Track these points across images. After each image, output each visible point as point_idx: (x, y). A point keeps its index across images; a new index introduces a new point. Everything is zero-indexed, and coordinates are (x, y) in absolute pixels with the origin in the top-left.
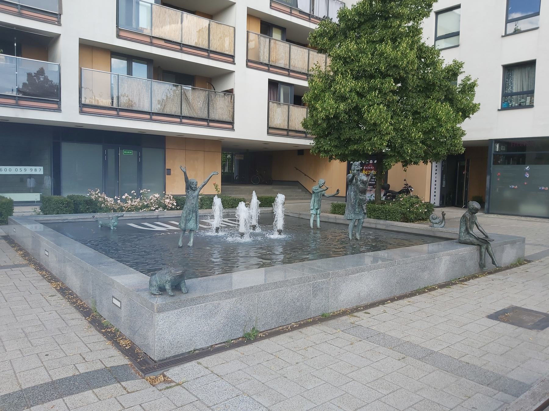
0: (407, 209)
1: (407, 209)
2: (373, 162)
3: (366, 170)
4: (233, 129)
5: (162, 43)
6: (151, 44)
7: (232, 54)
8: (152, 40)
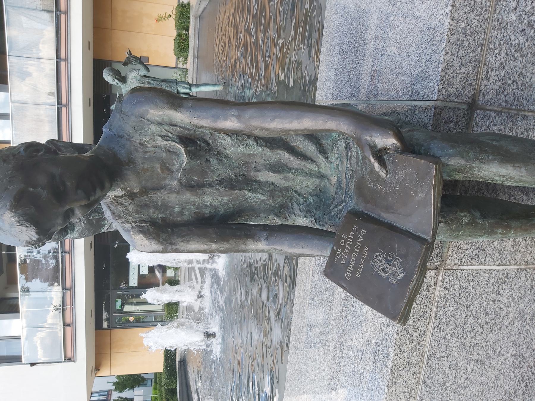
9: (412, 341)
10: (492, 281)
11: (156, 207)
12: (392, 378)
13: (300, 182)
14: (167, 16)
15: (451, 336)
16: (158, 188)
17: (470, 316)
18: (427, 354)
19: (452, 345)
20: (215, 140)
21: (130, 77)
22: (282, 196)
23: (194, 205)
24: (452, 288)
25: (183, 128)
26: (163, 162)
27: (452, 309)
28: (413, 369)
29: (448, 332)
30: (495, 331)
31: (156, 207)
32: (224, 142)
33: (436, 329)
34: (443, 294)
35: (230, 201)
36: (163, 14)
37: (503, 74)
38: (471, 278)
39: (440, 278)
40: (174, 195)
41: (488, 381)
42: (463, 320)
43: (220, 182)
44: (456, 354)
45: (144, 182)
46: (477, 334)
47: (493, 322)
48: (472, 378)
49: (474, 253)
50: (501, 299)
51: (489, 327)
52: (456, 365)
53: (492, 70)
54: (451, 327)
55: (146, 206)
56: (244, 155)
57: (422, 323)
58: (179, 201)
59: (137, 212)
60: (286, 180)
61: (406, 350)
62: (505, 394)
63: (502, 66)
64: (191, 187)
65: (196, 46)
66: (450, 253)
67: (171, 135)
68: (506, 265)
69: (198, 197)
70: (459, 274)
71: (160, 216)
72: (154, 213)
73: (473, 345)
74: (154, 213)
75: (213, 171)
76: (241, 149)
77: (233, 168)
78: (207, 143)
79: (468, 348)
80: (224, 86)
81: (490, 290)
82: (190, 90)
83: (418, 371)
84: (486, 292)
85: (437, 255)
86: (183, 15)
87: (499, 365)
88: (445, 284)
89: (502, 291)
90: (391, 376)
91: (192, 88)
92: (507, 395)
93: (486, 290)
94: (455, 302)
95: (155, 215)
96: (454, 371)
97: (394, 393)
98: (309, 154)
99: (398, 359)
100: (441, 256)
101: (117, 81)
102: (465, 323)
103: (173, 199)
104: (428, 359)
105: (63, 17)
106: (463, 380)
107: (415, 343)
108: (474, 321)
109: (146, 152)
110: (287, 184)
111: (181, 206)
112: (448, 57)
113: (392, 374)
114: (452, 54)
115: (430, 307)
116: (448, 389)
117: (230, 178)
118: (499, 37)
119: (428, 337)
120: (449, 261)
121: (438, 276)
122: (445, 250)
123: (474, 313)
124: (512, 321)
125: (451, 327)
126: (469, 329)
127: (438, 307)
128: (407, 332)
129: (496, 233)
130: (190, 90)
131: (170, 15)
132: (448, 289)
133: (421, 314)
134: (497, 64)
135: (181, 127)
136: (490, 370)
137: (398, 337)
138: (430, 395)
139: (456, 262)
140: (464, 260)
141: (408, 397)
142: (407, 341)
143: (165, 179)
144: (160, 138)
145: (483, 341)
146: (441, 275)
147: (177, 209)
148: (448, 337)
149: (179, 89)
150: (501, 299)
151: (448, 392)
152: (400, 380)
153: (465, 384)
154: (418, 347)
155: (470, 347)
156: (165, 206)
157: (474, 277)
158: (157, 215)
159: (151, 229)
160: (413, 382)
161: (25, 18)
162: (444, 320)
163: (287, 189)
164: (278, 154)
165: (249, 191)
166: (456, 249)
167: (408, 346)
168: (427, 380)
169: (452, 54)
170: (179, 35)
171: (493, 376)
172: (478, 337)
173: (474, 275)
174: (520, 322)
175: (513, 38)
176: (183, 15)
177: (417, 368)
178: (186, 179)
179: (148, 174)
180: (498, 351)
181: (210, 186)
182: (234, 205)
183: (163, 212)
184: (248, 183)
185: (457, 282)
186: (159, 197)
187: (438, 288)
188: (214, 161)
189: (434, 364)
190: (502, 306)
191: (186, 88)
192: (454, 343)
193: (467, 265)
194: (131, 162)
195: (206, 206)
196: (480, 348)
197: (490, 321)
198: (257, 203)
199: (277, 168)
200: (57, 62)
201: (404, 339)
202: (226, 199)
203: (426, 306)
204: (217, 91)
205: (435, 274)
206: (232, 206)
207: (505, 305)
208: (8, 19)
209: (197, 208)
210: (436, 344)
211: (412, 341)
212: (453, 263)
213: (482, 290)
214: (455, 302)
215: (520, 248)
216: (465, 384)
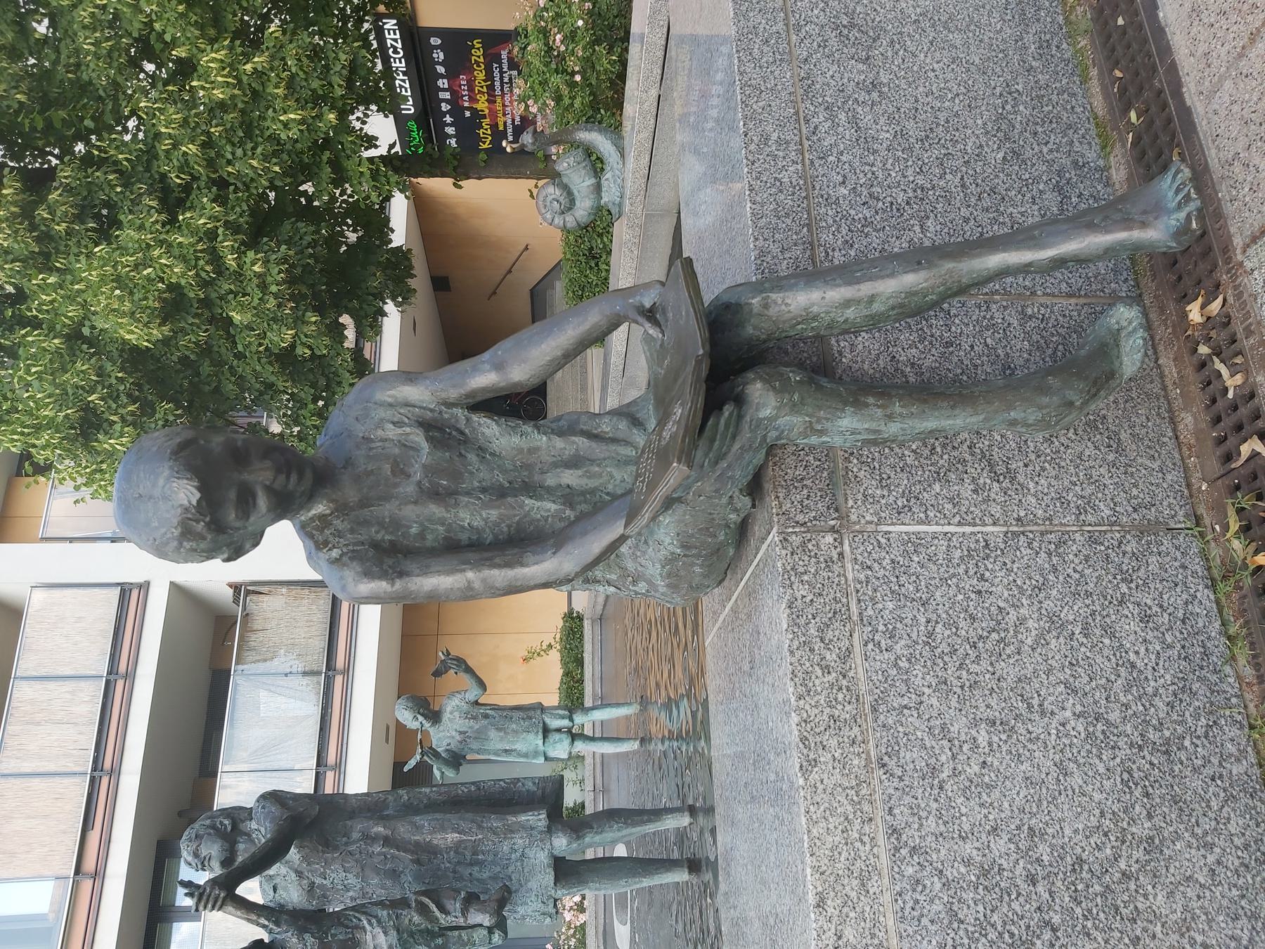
0: (572, 85)
1: (572, 85)
2: (442, 76)
3: (473, 99)
4: (144, 587)
5: (94, 837)
6: (99, 875)
7: (117, 591)
8: (87, 872)
9: (827, 670)
10: (958, 553)
11: (381, 524)
12: (805, 751)
13: (612, 477)
14: (544, 647)
15: (909, 660)
16: (387, 498)
17: (937, 622)
18: (869, 699)
19: (918, 681)
20: (474, 429)
21: (449, 709)
22: (585, 502)
23: (443, 524)
24: (876, 565)
25: (424, 408)
26: (395, 461)
27: (890, 605)
28: (846, 731)
29: (899, 652)
30: (1009, 656)
31: (381, 524)
32: (487, 431)
33: (870, 646)
34: (862, 577)
35: (502, 518)
36: (536, 645)
37: (853, 253)
38: (911, 548)
39: (846, 547)
40: (411, 507)
41: (1043, 776)
42: (922, 628)
43: (484, 490)
44: (934, 701)
45: (365, 490)
46: (967, 662)
47: (994, 636)
48: (996, 763)
49: (900, 504)
50: (993, 589)
51: (989, 646)
52: (943, 727)
53: (834, 250)
54: (903, 642)
55: (366, 523)
56: (521, 451)
57: (837, 633)
58: (418, 516)
59: (352, 531)
60: (589, 478)
61: (819, 689)
62: (1102, 814)
63: (848, 244)
64: (436, 495)
65: (598, 674)
66: (851, 503)
67: (406, 420)
68: (975, 525)
69: (448, 511)
70: (883, 541)
71: (387, 537)
72: (377, 532)
73: (968, 684)
74: (377, 532)
75: (471, 473)
76: (516, 440)
77: (504, 471)
78: (462, 433)
79: (959, 691)
80: (641, 704)
81: (961, 570)
82: (571, 720)
83: (860, 738)
84: (954, 575)
85: (828, 508)
86: (574, 633)
87: (1053, 737)
88: (859, 557)
89: (987, 574)
90: (801, 745)
91: (574, 717)
92: (1109, 816)
93: (952, 571)
94: (893, 592)
95: (379, 537)
96: (945, 742)
97: (821, 787)
98: (620, 435)
99: (807, 707)
100: (837, 510)
101: (421, 718)
102: (930, 635)
103: (410, 511)
104: (874, 710)
105: (339, 680)
106: (976, 768)
107: (834, 675)
108: (948, 632)
109: (371, 449)
110: (592, 483)
111: (422, 524)
112: (760, 243)
113: (803, 739)
114: (765, 240)
115: (844, 600)
116: (948, 787)
117: (501, 485)
118: (830, 213)
119: (859, 662)
120: (853, 518)
121: (841, 544)
122: (841, 499)
123: (944, 616)
124: (1041, 636)
125: (903, 642)
126: (944, 647)
127: (859, 601)
128: (812, 650)
129: (867, 405)
130: (571, 720)
131: (550, 646)
132: (869, 567)
133: (830, 615)
134: (839, 242)
135: (421, 407)
136: (1035, 747)
137: (793, 660)
138: (907, 799)
139: (868, 518)
140: (883, 515)
141: (855, 798)
142: (817, 668)
143: (396, 485)
144: (391, 426)
145: (987, 676)
146: (846, 542)
147: (414, 530)
148: (903, 664)
149: (548, 721)
150: (993, 589)
151: (950, 794)
152: (825, 757)
153: (987, 779)
154: (845, 683)
155: (962, 687)
156: (396, 524)
157: (916, 546)
158: (385, 536)
159: (371, 553)
160: (856, 762)
161: (265, 693)
162: (881, 628)
163: (593, 492)
164: (574, 442)
165: (531, 497)
166: (860, 496)
167: (821, 681)
168: (886, 758)
169: (765, 240)
170: (567, 674)
171: (1050, 763)
172: (974, 668)
173: (914, 544)
174: (1062, 640)
175: (852, 212)
176: (574, 633)
177: (856, 730)
178: (430, 482)
179: (372, 478)
180: (1035, 702)
181: (468, 494)
182: (509, 526)
183: (391, 533)
184: (532, 489)
185: (884, 554)
186: (387, 510)
187: (849, 566)
188: (472, 457)
189: (891, 722)
190: (1002, 604)
191: (563, 717)
192: (919, 677)
193: (893, 524)
194: (348, 463)
195: (463, 527)
196: (987, 692)
197: (985, 634)
198: (546, 520)
199: (574, 462)
200: (317, 774)
201: (808, 664)
202: (494, 514)
203: (835, 599)
204: (627, 718)
205: (835, 540)
206: (505, 529)
207: (1006, 601)
208: (234, 699)
209: (448, 531)
210: (880, 677)
211: (827, 670)
212: (863, 521)
213: (942, 570)
214: (893, 592)
215: (993, 495)
216: (987, 779)
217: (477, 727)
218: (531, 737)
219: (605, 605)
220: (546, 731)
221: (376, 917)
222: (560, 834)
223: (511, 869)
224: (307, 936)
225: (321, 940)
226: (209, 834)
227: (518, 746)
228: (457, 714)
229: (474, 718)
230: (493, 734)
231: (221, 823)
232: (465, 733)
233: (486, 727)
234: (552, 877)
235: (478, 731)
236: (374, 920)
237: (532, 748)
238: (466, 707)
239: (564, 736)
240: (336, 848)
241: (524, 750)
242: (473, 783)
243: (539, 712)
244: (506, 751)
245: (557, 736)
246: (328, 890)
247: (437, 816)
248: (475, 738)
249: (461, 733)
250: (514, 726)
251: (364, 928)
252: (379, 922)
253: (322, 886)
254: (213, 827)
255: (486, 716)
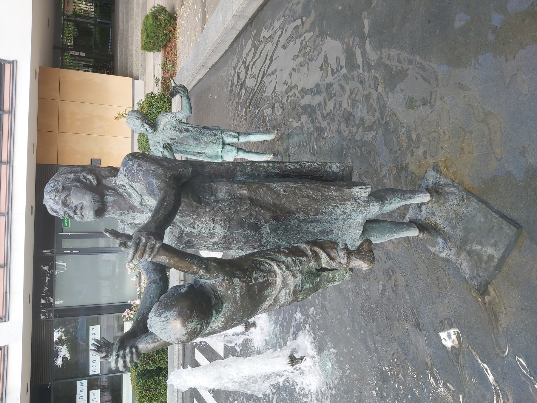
101: (146, 126)
149: (225, 138)
191: (234, 137)
217: (181, 136)
218: (215, 146)
219: (194, 87)
220: (224, 144)
221: (283, 263)
222: (375, 203)
223: (334, 226)
224: (236, 281)
225: (247, 282)
226: (77, 187)
227: (206, 151)
228: (168, 127)
229: (180, 131)
230: (191, 142)
231: (85, 177)
232: (174, 139)
233: (186, 137)
234: (360, 233)
235: (182, 139)
236: (282, 266)
237: (214, 153)
238: (174, 122)
239: (233, 148)
240: (207, 204)
241: (210, 154)
242: (296, 163)
243: (220, 132)
244: (199, 153)
245: (229, 148)
246: (194, 237)
247: (290, 184)
248: (181, 143)
249: (171, 139)
250: (205, 139)
251: (274, 272)
252: (288, 267)
253: (189, 234)
254: (78, 180)
255: (188, 131)
